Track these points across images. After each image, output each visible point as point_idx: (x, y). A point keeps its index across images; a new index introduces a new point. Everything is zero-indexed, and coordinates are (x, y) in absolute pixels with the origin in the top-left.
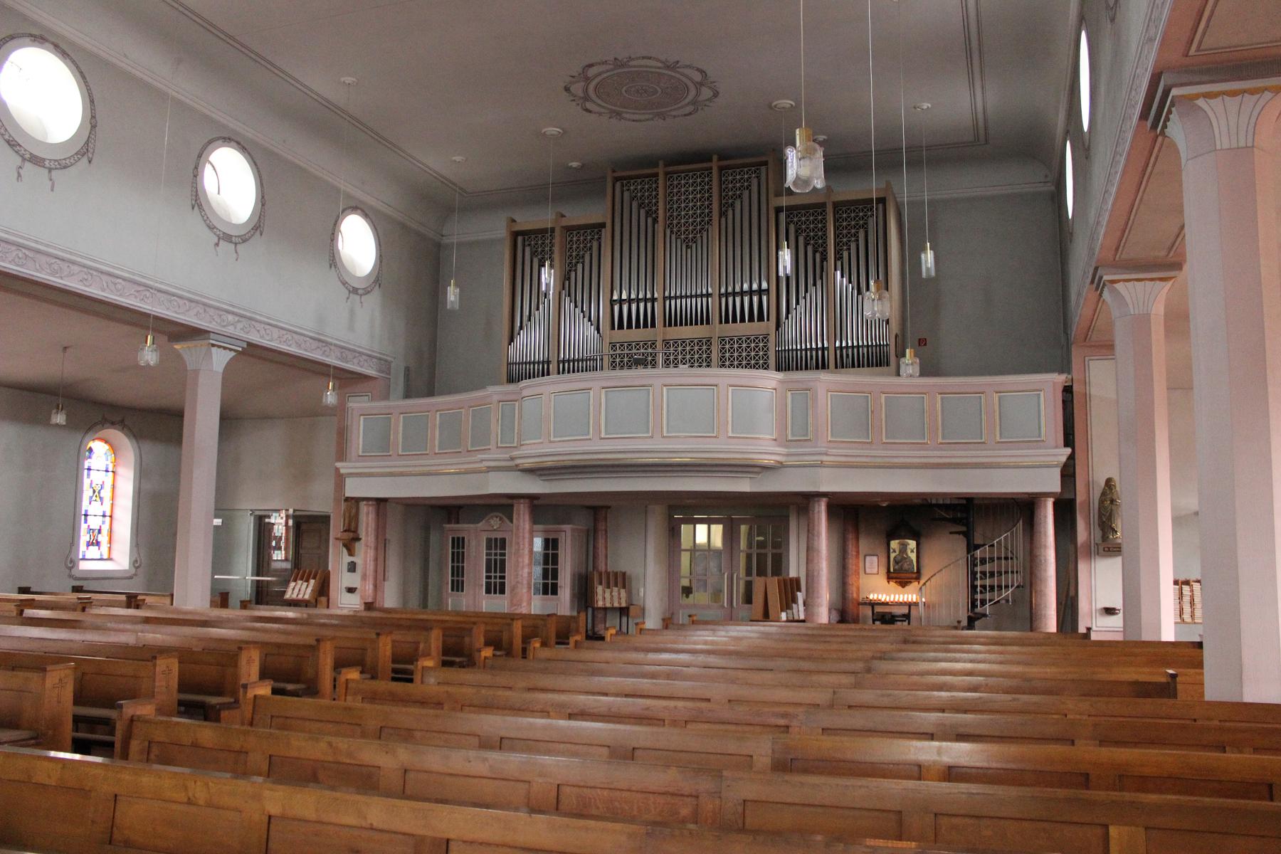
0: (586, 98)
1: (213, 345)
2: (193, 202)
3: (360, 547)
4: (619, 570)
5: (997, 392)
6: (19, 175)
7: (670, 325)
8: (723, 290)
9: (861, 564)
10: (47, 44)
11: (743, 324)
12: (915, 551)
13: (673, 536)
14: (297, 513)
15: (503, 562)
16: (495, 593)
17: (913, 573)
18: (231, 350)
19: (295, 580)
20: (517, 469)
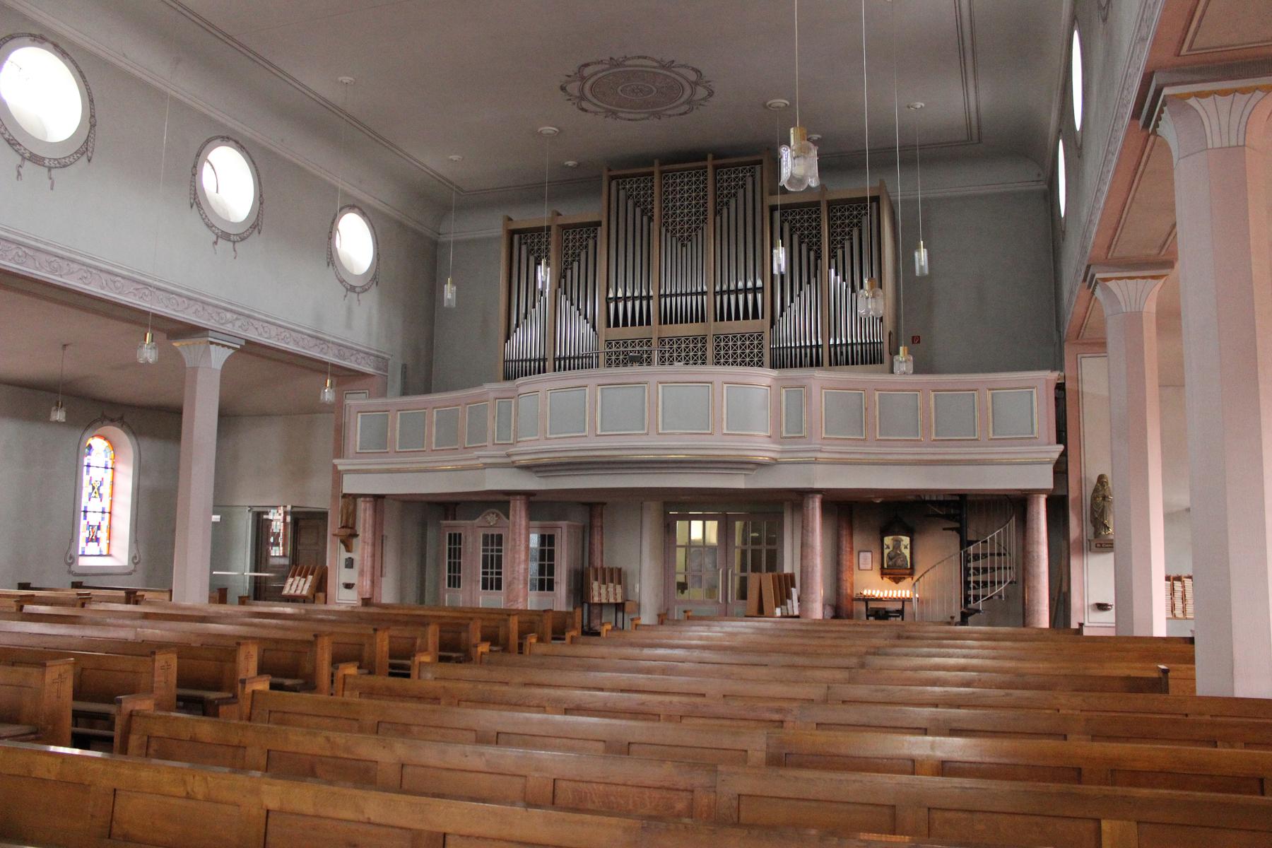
0: (582, 97)
1: (212, 343)
2: (192, 201)
3: (357, 543)
4: (614, 566)
5: (990, 390)
6: (19, 174)
7: (665, 323)
8: (718, 288)
9: (855, 561)
10: (47, 44)
11: (738, 322)
12: (909, 547)
13: (668, 532)
14: (295, 510)
15: (499, 558)
16: (492, 589)
17: (906, 569)
18: (229, 347)
19: (293, 576)
20: (514, 465)
